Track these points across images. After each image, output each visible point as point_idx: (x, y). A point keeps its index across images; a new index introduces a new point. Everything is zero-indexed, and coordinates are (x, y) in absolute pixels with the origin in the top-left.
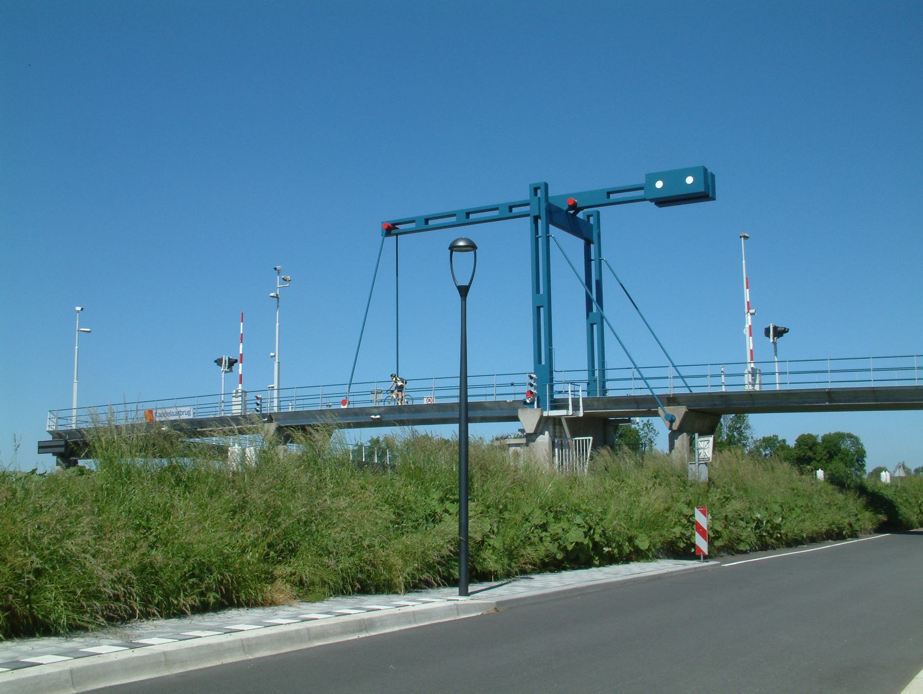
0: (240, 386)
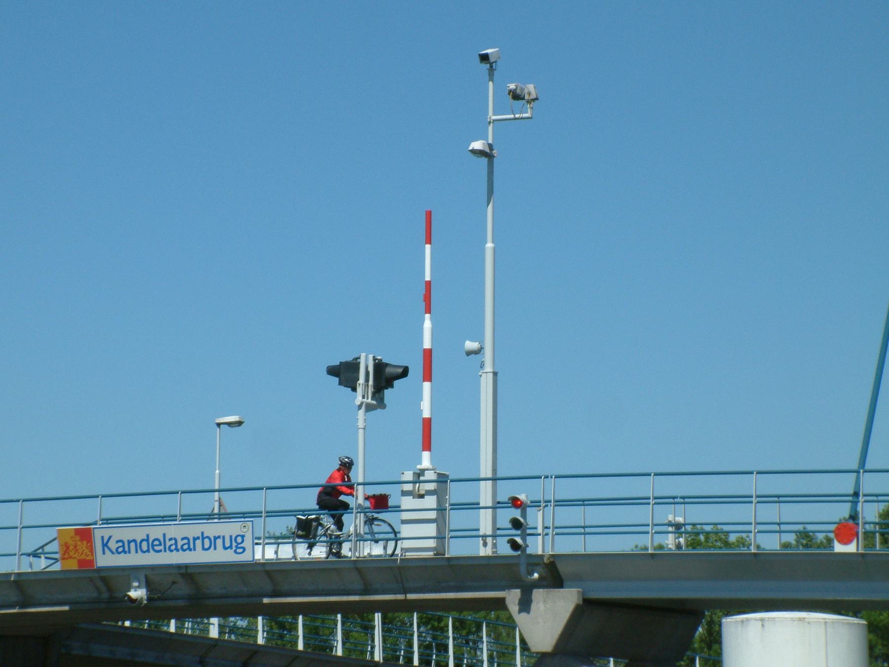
0: (426, 460)
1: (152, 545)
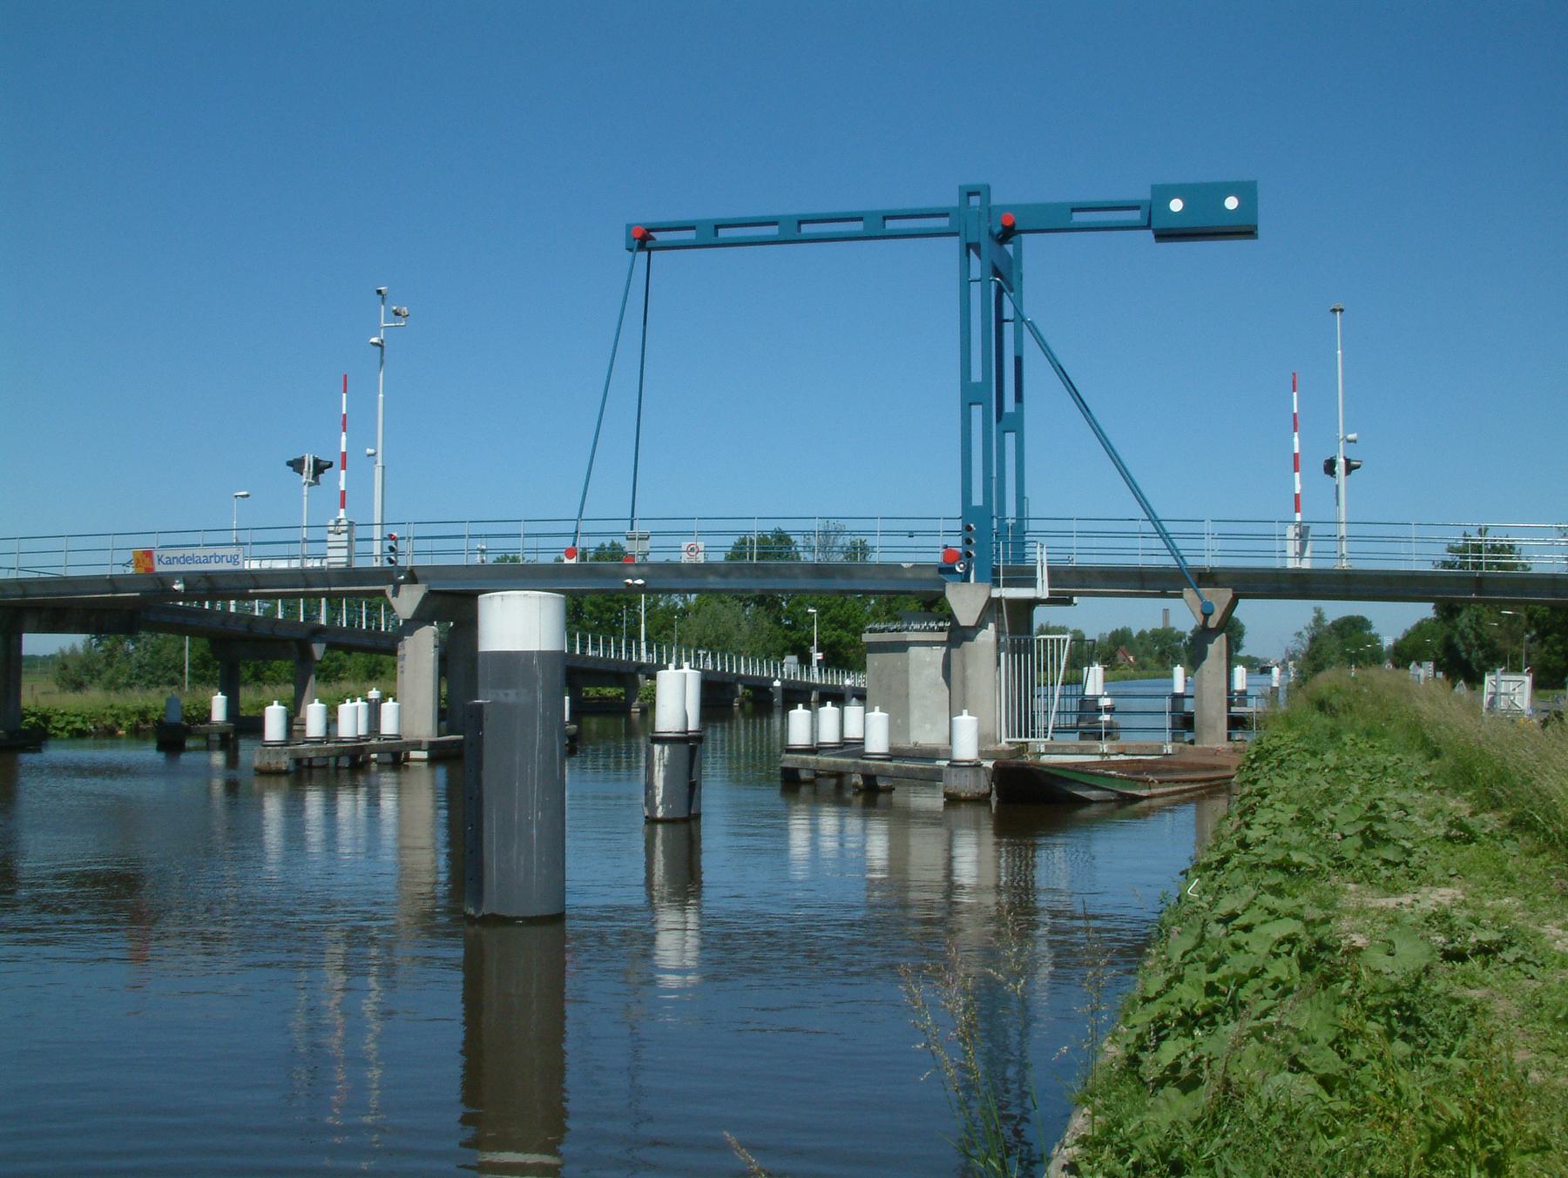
0: (342, 514)
1: (186, 560)
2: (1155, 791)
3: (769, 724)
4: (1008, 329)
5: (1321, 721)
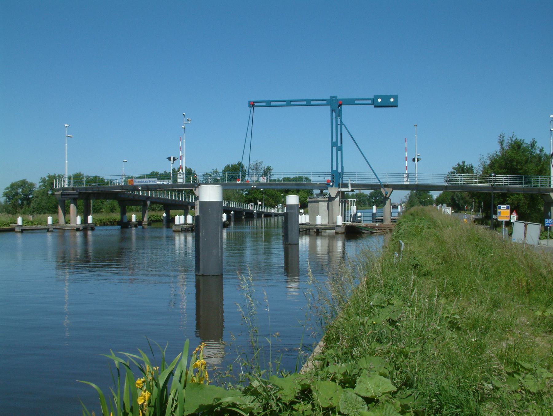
2: (377, 231)
3: (253, 223)
4: (339, 126)
5: (411, 217)
